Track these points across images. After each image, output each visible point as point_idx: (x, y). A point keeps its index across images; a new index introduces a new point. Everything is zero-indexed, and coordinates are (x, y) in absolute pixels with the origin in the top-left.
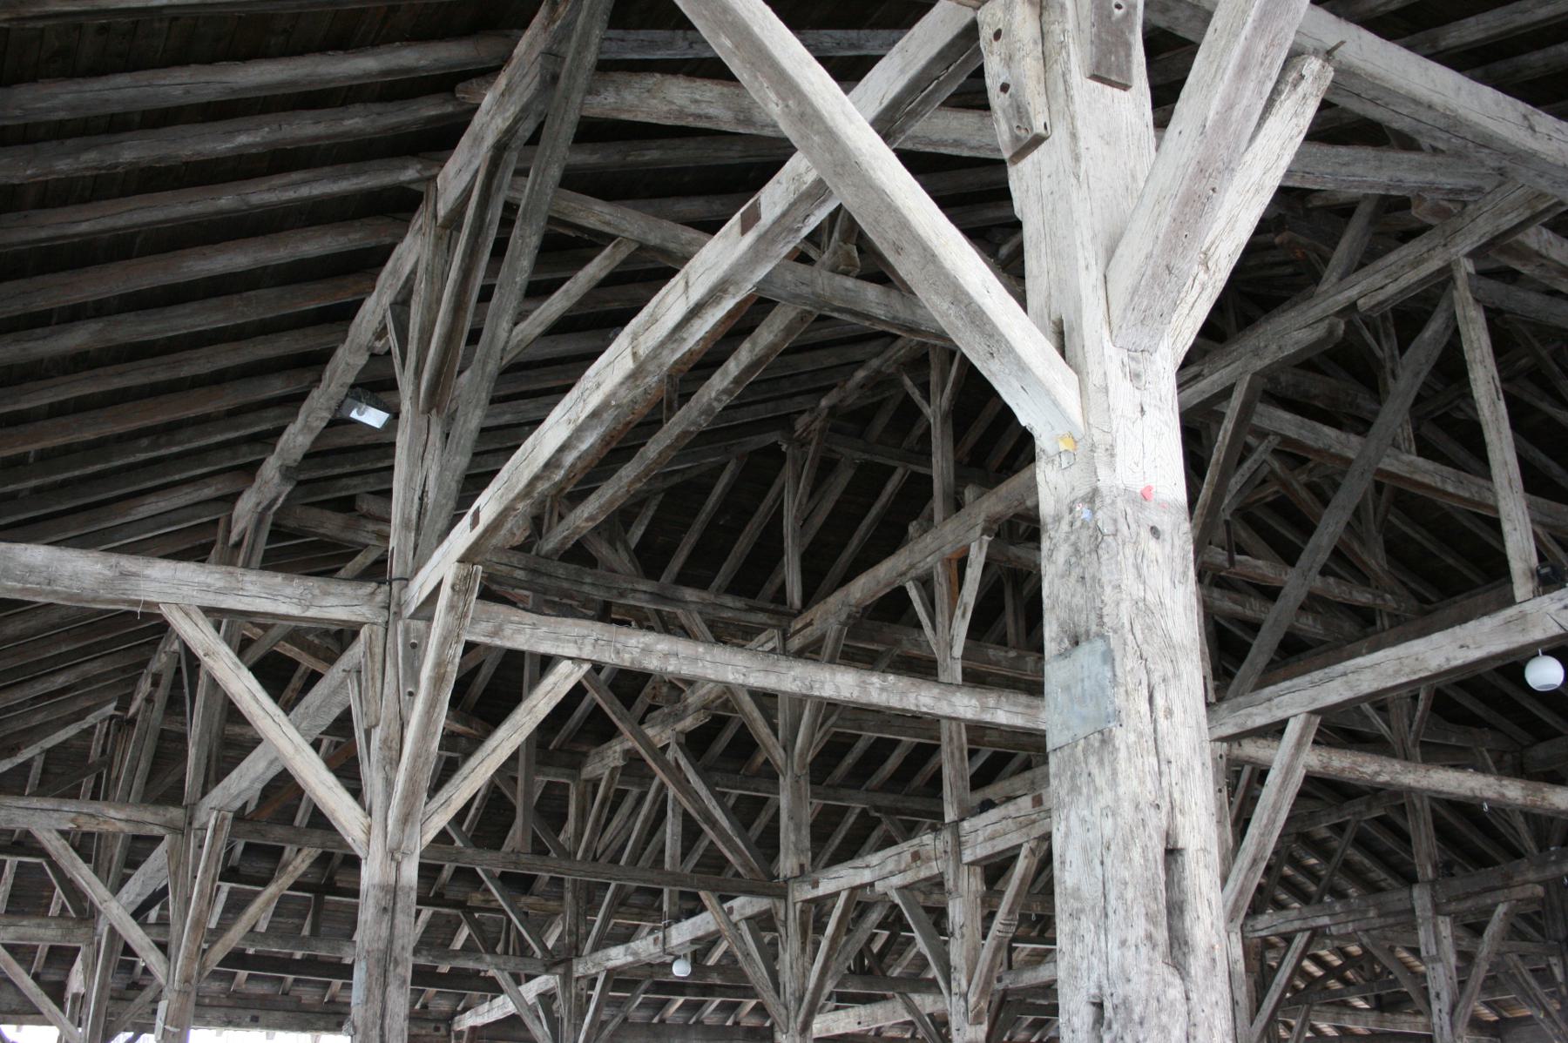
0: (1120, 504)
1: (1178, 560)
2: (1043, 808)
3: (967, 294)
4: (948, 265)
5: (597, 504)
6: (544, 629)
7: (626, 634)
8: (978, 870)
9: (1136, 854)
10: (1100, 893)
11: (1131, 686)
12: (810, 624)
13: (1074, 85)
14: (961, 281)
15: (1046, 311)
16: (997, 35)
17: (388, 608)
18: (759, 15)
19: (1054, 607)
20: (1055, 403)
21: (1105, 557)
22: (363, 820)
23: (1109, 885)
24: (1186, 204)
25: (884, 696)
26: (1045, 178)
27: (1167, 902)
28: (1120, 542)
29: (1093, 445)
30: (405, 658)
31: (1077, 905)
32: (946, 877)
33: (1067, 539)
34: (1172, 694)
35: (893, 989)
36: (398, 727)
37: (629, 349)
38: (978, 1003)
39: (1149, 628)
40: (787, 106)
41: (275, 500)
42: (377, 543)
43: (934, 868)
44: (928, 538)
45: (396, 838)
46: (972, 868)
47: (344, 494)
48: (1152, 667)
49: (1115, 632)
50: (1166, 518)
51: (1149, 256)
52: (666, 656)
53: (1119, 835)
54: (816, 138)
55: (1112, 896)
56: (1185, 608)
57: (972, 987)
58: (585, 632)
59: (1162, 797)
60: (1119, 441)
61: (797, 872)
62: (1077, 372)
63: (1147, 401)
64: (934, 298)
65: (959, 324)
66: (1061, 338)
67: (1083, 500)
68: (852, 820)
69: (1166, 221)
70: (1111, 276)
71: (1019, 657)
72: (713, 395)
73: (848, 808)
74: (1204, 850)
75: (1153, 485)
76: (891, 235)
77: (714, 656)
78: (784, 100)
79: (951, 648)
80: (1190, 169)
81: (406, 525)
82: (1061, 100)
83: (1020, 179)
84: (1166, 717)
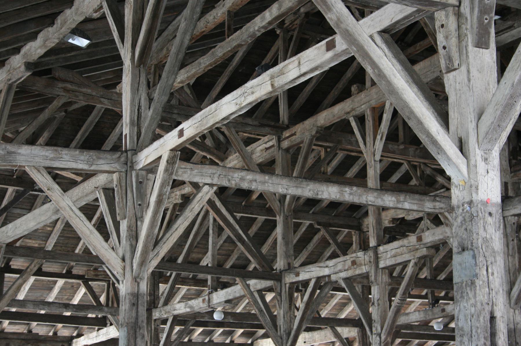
0: (479, 206)
1: (497, 223)
2: (422, 243)
3: (432, 136)
4: (426, 126)
5: (186, 76)
6: (196, 171)
7: (233, 172)
8: (387, 271)
9: (481, 319)
10: (470, 329)
11: (481, 266)
12: (294, 134)
13: (469, 51)
14: (430, 131)
15: (456, 133)
16: (442, 26)
17: (127, 164)
18: (366, 41)
19: (456, 237)
20: (459, 171)
21: (474, 224)
22: (121, 264)
23: (473, 328)
24: (506, 107)
25: (351, 197)
26: (457, 84)
27: (490, 333)
28: (479, 219)
29: (471, 185)
30: (137, 188)
31: (462, 333)
32: (370, 275)
33: (461, 215)
34: (494, 267)
35: (327, 325)
36: (135, 220)
37: (269, 82)
38: (386, 339)
39: (487, 247)
40: (374, 71)
41: (21, 78)
42: (64, 94)
43: (364, 269)
44: (363, 95)
45: (138, 272)
46: (384, 271)
47: (46, 68)
48: (488, 259)
49: (477, 248)
50: (494, 209)
51: (492, 123)
52: (251, 181)
53: (476, 313)
54: (384, 82)
55: (474, 331)
56: (499, 238)
57: (384, 331)
58: (215, 172)
59: (490, 301)
60: (480, 184)
61: (287, 267)
62: (466, 158)
63: (489, 168)
64: (420, 134)
65: (428, 143)
66: (462, 146)
67: (467, 203)
68: (304, 229)
69: (499, 112)
70: (479, 125)
71: (405, 148)
72: (256, 28)
73: (301, 223)
74: (502, 317)
75: (490, 198)
76: (407, 114)
77: (272, 180)
78: (373, 69)
79: (374, 155)
80: (508, 97)
81: (132, 123)
82: (465, 56)
83: (448, 80)
84: (492, 275)
